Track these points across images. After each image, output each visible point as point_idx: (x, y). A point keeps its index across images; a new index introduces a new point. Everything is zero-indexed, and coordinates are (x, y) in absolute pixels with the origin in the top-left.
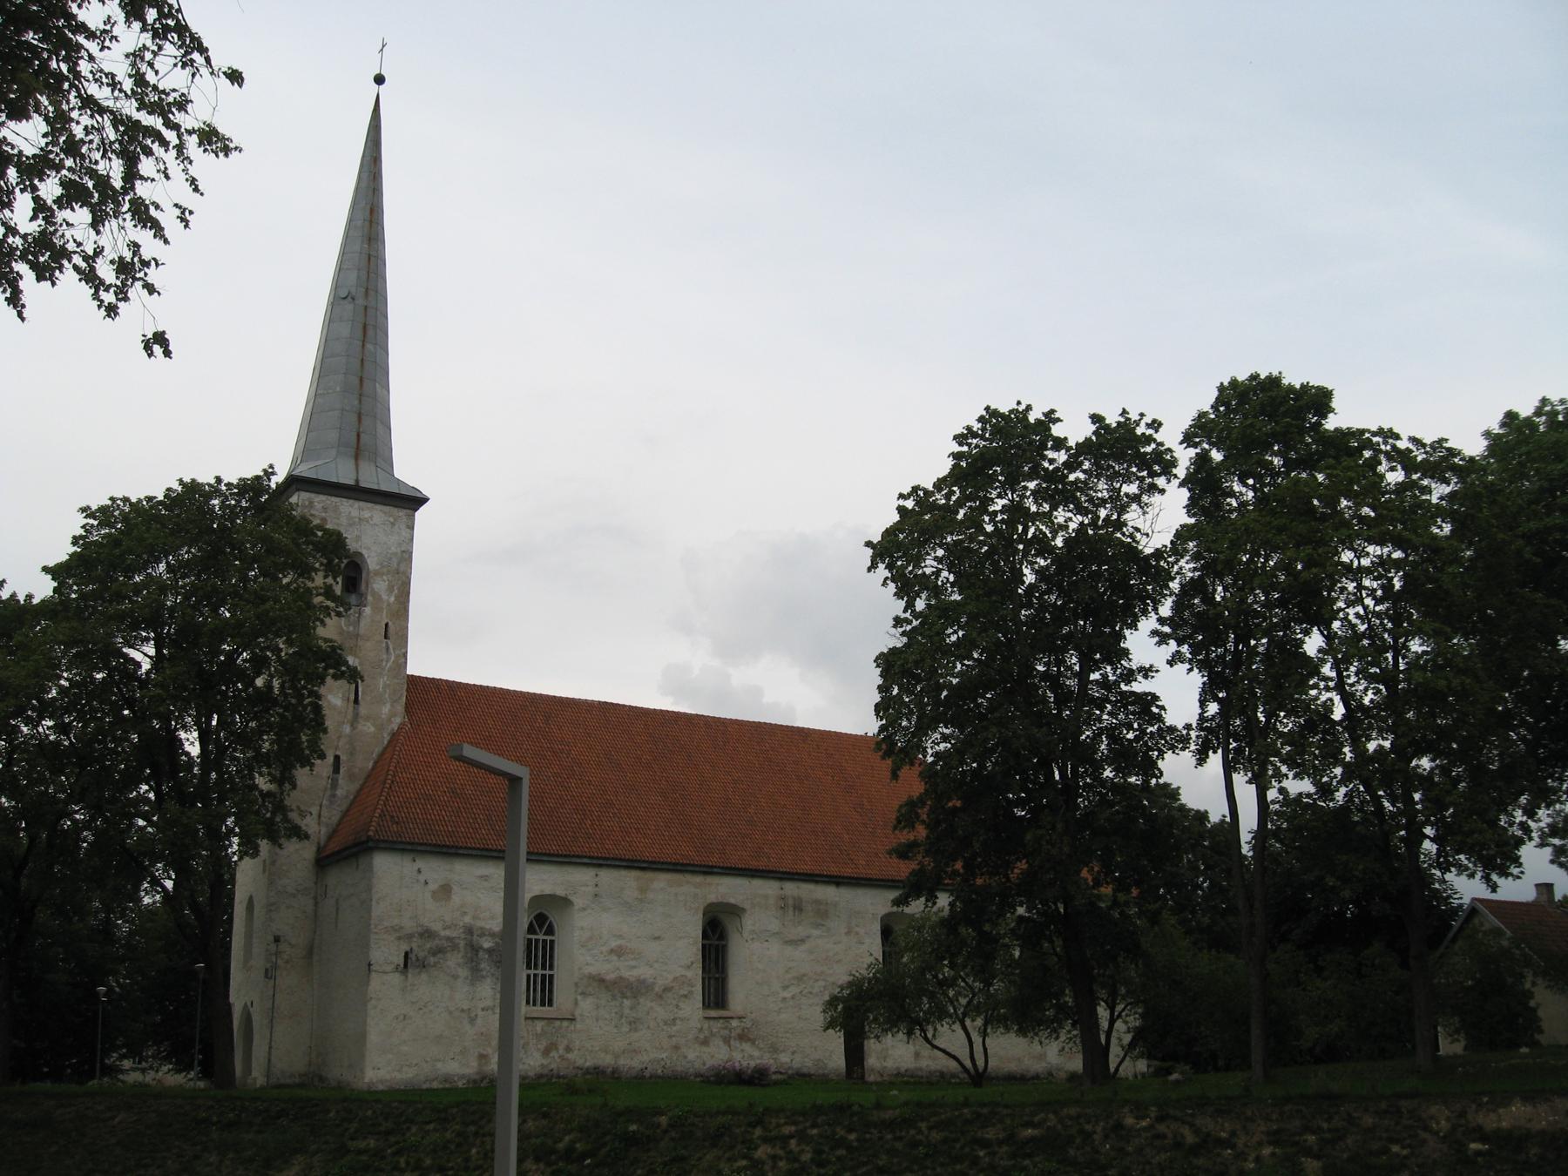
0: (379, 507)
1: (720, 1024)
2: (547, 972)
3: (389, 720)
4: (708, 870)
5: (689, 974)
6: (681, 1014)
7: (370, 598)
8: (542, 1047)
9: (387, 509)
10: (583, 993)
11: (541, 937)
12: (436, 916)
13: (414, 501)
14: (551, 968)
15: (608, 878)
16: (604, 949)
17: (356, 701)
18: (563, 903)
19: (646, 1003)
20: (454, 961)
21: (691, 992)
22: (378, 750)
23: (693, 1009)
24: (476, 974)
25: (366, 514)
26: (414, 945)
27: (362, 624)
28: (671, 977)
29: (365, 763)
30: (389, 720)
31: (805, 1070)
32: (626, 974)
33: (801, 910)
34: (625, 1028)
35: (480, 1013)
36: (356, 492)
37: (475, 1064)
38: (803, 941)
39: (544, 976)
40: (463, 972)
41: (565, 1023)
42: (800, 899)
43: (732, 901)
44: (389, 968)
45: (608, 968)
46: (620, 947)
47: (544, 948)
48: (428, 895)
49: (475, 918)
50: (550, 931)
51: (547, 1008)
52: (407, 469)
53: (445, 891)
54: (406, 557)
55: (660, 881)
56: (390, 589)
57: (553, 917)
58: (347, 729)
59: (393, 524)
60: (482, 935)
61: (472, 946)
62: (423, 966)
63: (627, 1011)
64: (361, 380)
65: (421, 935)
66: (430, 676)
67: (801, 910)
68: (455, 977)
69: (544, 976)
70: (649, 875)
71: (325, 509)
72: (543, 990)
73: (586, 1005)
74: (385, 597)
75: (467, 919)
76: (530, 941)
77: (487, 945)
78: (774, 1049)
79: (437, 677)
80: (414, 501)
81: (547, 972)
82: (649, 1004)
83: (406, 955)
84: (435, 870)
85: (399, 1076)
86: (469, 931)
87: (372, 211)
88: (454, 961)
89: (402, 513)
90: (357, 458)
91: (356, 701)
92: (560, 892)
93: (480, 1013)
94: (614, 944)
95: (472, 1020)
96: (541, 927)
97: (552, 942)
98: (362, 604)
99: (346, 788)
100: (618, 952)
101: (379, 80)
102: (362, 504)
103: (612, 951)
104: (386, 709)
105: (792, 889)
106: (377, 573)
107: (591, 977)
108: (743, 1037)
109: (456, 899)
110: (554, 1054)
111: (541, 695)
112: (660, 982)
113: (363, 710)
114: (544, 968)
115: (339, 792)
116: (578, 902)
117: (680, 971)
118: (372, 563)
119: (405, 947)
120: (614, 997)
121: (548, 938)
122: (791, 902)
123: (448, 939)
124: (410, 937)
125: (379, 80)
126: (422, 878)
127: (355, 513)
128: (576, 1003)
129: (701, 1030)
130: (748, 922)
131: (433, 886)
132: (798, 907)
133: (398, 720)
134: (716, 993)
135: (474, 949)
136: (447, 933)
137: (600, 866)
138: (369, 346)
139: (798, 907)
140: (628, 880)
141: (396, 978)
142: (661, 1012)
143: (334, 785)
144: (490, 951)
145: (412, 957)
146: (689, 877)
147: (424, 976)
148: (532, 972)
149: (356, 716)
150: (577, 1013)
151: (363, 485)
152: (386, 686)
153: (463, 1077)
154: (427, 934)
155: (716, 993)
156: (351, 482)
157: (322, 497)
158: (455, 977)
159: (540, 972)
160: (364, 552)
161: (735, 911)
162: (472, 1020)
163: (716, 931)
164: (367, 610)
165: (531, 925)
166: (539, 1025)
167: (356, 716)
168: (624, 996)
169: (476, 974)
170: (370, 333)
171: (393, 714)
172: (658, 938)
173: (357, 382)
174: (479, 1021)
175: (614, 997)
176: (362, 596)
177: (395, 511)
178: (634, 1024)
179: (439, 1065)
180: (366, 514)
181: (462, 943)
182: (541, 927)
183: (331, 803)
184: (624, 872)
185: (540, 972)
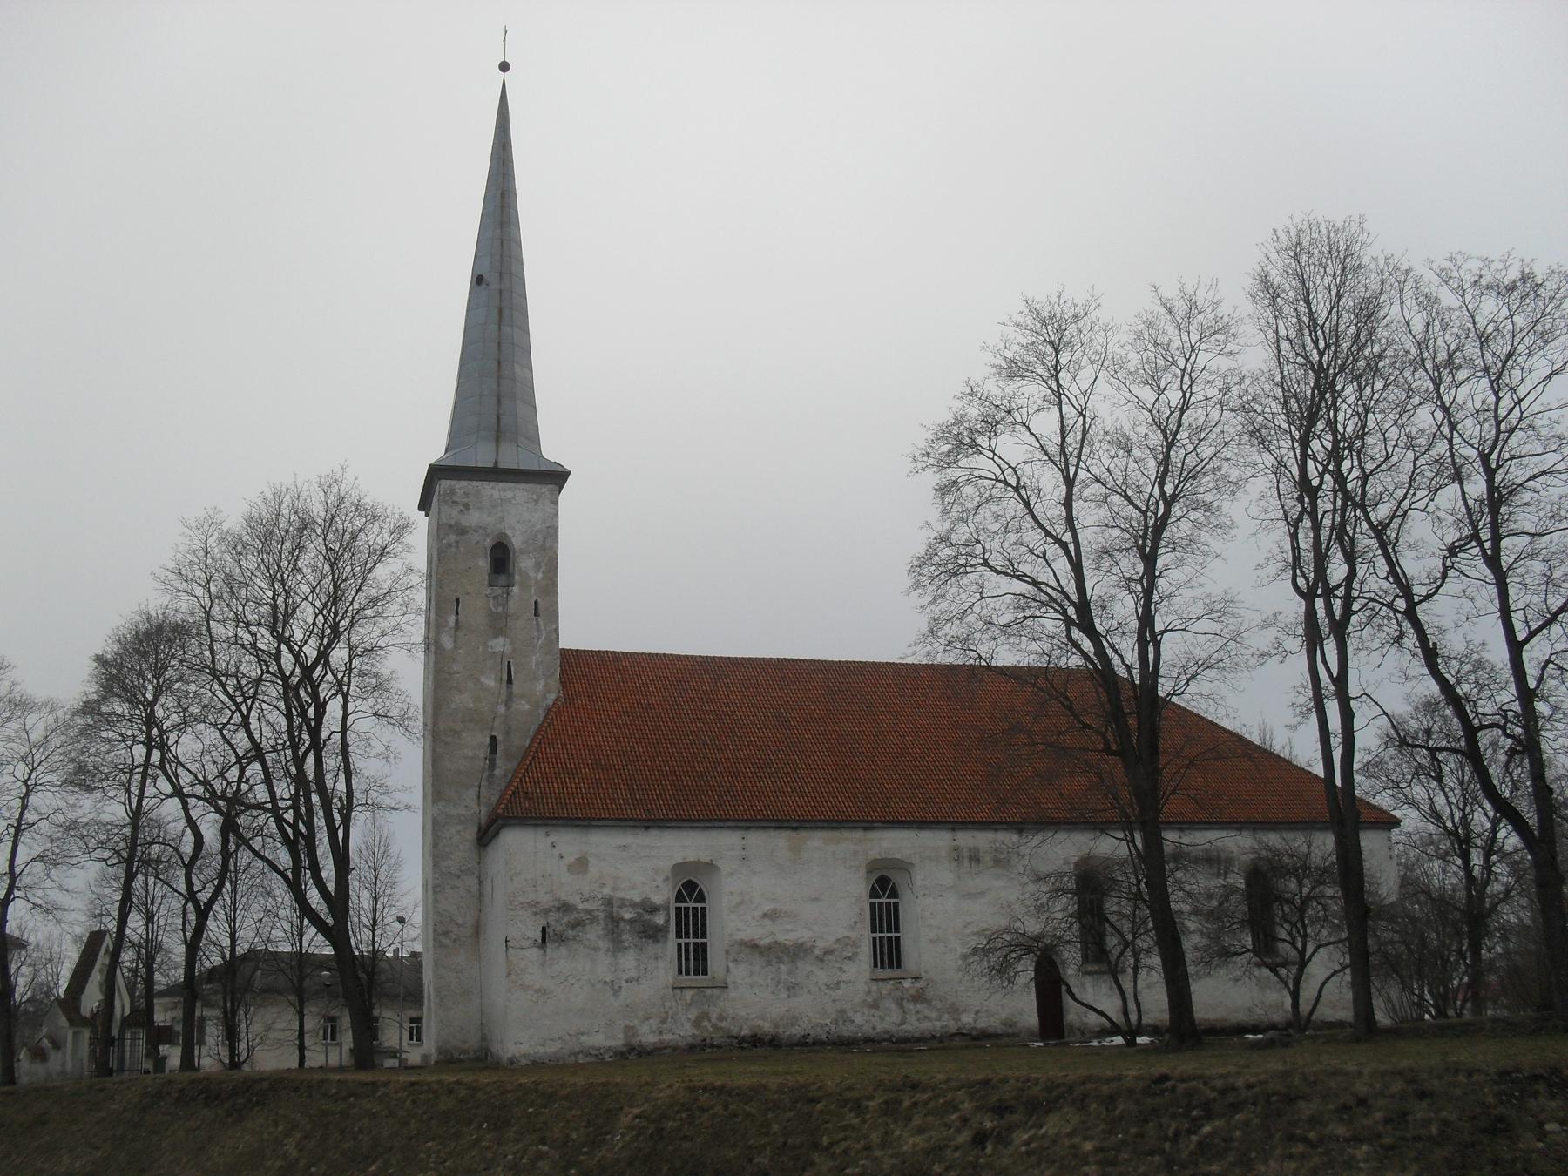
0: (522, 486)
1: (889, 986)
2: (700, 940)
3: (544, 697)
4: (868, 825)
5: (853, 935)
6: (844, 977)
7: (517, 577)
8: (692, 1016)
9: (527, 486)
10: (735, 960)
11: (691, 905)
12: (572, 888)
13: (558, 477)
15: (757, 840)
16: (758, 913)
17: (510, 681)
18: (710, 867)
19: (805, 966)
20: (593, 934)
21: (856, 954)
22: (534, 728)
23: (861, 968)
24: (617, 946)
25: (509, 494)
26: (551, 920)
27: (511, 603)
28: (832, 939)
29: (521, 741)
30: (544, 697)
31: (991, 1030)
32: (781, 938)
33: (978, 860)
34: (784, 994)
35: (624, 984)
36: (496, 474)
37: (621, 1036)
38: (982, 893)
40: (604, 944)
41: (716, 991)
42: (977, 850)
43: (898, 856)
44: (525, 943)
45: (761, 933)
46: (774, 911)
47: (695, 916)
48: (565, 869)
49: (614, 889)
51: (701, 977)
52: (552, 449)
53: (581, 865)
54: (552, 532)
55: (816, 841)
56: (538, 566)
57: (703, 884)
58: (502, 709)
59: (536, 501)
60: (623, 905)
61: (612, 919)
62: (561, 939)
63: (784, 977)
64: (499, 364)
65: (558, 909)
66: (836, 659)
67: (978, 860)
68: (596, 949)
69: (890, 939)
70: (804, 834)
71: (466, 494)
72: (696, 959)
73: (739, 973)
74: (532, 575)
75: (606, 891)
77: (627, 916)
78: (955, 1011)
79: (603, 649)
80: (558, 477)
81: (700, 940)
82: (809, 968)
83: (544, 929)
84: (569, 842)
85: (542, 1050)
86: (608, 902)
87: (503, 195)
88: (593, 934)
89: (545, 489)
90: (497, 440)
91: (510, 681)
92: (705, 858)
93: (624, 984)
94: (767, 907)
95: (616, 992)
96: (690, 896)
97: (704, 909)
98: (510, 585)
99: (502, 767)
100: (771, 916)
101: (504, 67)
102: (501, 485)
103: (765, 915)
104: (540, 686)
105: (966, 839)
106: (523, 552)
107: (743, 943)
108: (918, 998)
109: (593, 870)
110: (706, 1023)
112: (821, 944)
113: (516, 689)
114: (695, 936)
115: (497, 772)
116: (725, 866)
117: (842, 933)
118: (517, 542)
119: (544, 923)
120: (769, 963)
121: (699, 905)
122: (966, 853)
123: (589, 912)
124: (546, 911)
125: (504, 67)
126: (556, 852)
127: (496, 495)
128: (728, 971)
129: (869, 992)
130: (919, 877)
131: (569, 859)
132: (975, 858)
133: (553, 696)
134: (888, 954)
135: (614, 921)
136: (587, 906)
137: (748, 828)
138: (506, 329)
139: (975, 858)
140: (779, 841)
141: (534, 953)
142: (822, 976)
143: (492, 766)
144: (632, 921)
145: (550, 931)
146: (847, 834)
147: (563, 950)
148: (683, 941)
149: (510, 696)
150: (729, 981)
151: (501, 466)
152: (538, 663)
153: (609, 1049)
154: (565, 908)
155: (888, 954)
156: (490, 465)
157: (464, 483)
158: (596, 949)
159: (691, 940)
160: (509, 532)
161: (904, 867)
162: (616, 992)
163: (885, 887)
164: (516, 589)
165: (873, 888)
166: (688, 994)
167: (510, 696)
168: (780, 961)
169: (617, 946)
170: (506, 313)
171: (547, 690)
172: (816, 899)
173: (495, 365)
174: (623, 993)
175: (769, 963)
176: (510, 576)
177: (538, 488)
178: (792, 988)
179: (584, 1038)
180: (509, 494)
181: (602, 915)
182: (690, 896)
183: (490, 783)
184: (773, 833)
185: (691, 940)
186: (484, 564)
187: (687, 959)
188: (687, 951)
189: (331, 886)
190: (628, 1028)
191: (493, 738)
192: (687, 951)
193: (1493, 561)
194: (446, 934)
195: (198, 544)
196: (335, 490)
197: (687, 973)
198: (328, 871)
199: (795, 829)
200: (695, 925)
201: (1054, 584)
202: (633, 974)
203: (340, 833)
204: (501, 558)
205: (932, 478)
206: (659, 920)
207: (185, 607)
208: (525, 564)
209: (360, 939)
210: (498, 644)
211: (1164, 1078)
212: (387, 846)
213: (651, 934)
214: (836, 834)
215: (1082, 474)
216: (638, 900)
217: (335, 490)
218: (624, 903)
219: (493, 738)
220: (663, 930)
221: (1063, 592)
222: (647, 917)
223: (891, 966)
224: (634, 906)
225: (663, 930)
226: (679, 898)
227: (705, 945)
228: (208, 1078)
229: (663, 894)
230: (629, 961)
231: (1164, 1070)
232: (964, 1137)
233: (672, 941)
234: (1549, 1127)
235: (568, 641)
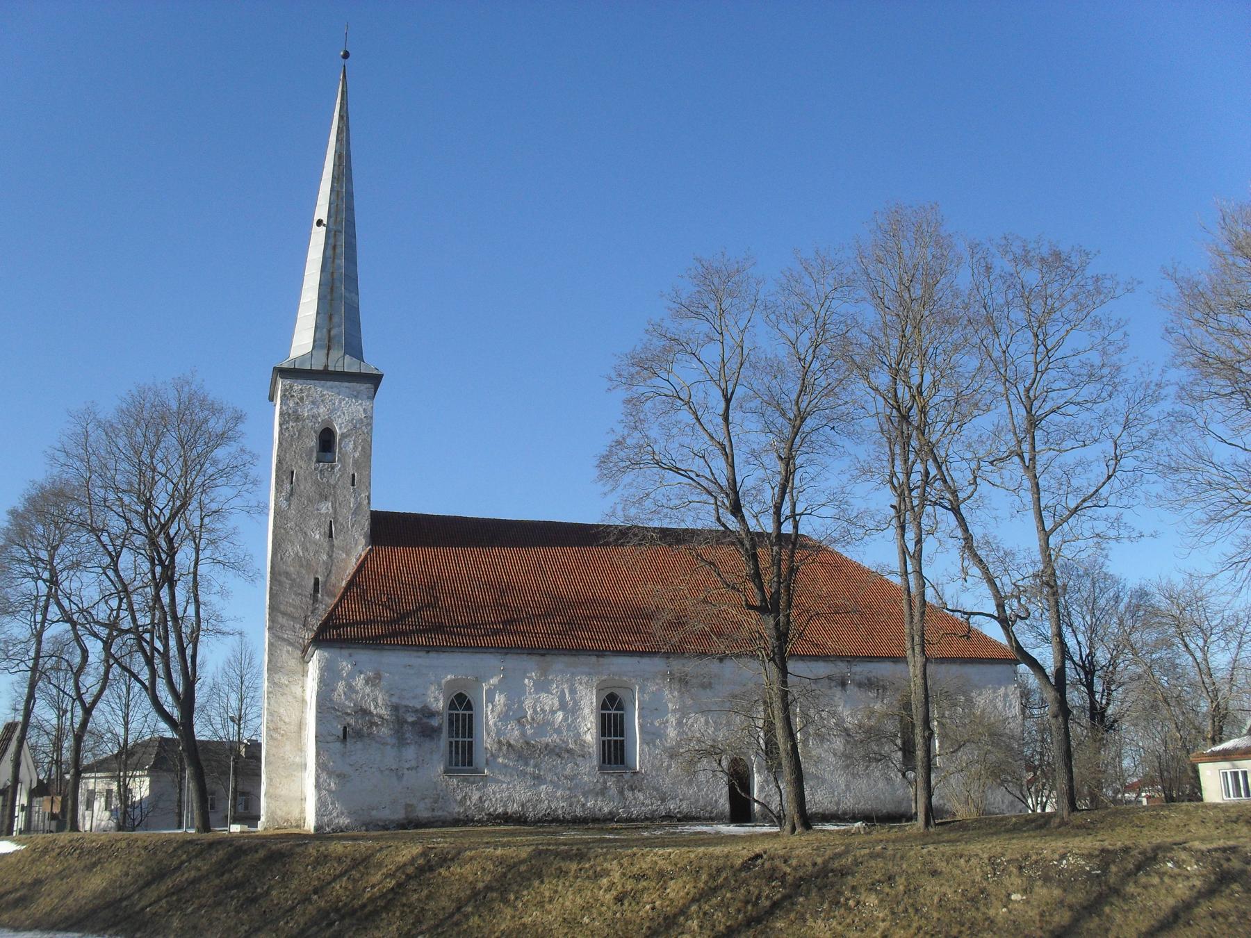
2: (467, 739)
14: (622, 735)
24: (401, 742)
39: (457, 742)
47: (464, 720)
50: (620, 707)
57: (470, 695)
62: (359, 735)
68: (385, 744)
69: (616, 742)
70: (549, 658)
72: (463, 753)
76: (451, 715)
77: (410, 719)
81: (467, 739)
91: (331, 536)
93: (406, 772)
95: (400, 778)
96: (461, 704)
97: (471, 716)
111: (477, 519)
144: (413, 724)
146: (583, 659)
147: (359, 745)
159: (460, 739)
162: (400, 778)
169: (401, 742)
179: (374, 813)
182: (461, 704)
185: (460, 739)
186: (312, 442)
187: (457, 753)
188: (457, 747)
189: (180, 688)
190: (407, 806)
191: (317, 580)
192: (457, 747)
193: (1030, 468)
194: (275, 730)
195: (79, 430)
196: (186, 389)
197: (456, 765)
198: (177, 678)
199: (543, 655)
200: (464, 727)
201: (709, 475)
202: (413, 763)
203: (189, 652)
204: (327, 441)
205: (622, 394)
206: (435, 722)
207: (72, 475)
208: (348, 448)
209: (202, 732)
210: (326, 507)
211: (758, 856)
212: (251, 658)
213: (427, 733)
214: (572, 659)
215: (740, 391)
216: (419, 706)
217: (186, 389)
218: (408, 709)
219: (317, 580)
220: (437, 731)
221: (716, 482)
222: (425, 720)
223: (616, 763)
224: (416, 711)
225: (437, 731)
226: (452, 706)
227: (622, 742)
228: (284, 850)
229: (439, 703)
230: (410, 753)
231: (758, 850)
232: (609, 897)
233: (444, 739)
234: (1014, 897)
235: (377, 506)
